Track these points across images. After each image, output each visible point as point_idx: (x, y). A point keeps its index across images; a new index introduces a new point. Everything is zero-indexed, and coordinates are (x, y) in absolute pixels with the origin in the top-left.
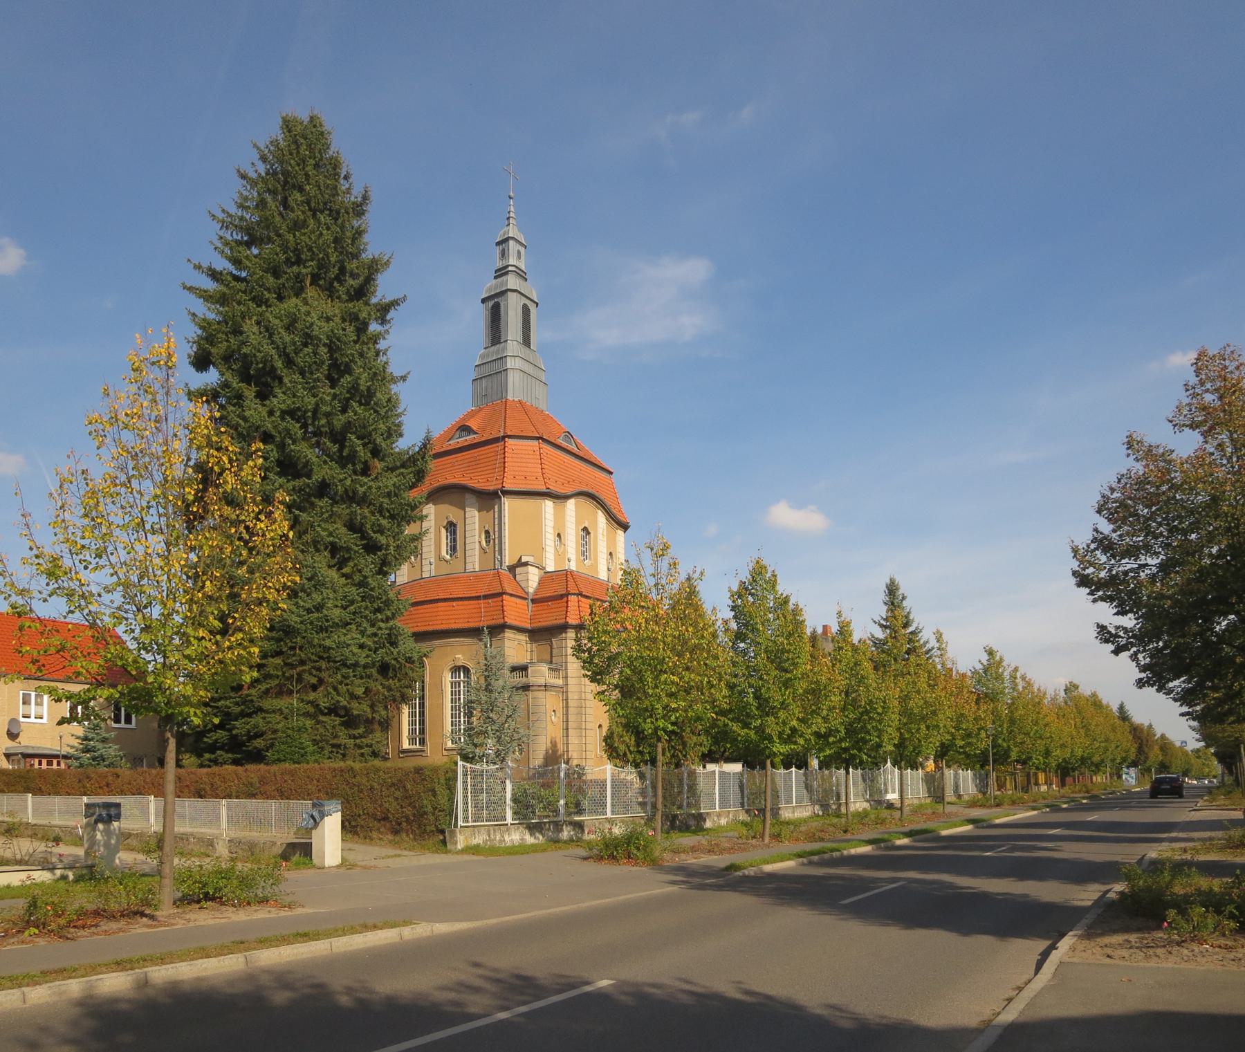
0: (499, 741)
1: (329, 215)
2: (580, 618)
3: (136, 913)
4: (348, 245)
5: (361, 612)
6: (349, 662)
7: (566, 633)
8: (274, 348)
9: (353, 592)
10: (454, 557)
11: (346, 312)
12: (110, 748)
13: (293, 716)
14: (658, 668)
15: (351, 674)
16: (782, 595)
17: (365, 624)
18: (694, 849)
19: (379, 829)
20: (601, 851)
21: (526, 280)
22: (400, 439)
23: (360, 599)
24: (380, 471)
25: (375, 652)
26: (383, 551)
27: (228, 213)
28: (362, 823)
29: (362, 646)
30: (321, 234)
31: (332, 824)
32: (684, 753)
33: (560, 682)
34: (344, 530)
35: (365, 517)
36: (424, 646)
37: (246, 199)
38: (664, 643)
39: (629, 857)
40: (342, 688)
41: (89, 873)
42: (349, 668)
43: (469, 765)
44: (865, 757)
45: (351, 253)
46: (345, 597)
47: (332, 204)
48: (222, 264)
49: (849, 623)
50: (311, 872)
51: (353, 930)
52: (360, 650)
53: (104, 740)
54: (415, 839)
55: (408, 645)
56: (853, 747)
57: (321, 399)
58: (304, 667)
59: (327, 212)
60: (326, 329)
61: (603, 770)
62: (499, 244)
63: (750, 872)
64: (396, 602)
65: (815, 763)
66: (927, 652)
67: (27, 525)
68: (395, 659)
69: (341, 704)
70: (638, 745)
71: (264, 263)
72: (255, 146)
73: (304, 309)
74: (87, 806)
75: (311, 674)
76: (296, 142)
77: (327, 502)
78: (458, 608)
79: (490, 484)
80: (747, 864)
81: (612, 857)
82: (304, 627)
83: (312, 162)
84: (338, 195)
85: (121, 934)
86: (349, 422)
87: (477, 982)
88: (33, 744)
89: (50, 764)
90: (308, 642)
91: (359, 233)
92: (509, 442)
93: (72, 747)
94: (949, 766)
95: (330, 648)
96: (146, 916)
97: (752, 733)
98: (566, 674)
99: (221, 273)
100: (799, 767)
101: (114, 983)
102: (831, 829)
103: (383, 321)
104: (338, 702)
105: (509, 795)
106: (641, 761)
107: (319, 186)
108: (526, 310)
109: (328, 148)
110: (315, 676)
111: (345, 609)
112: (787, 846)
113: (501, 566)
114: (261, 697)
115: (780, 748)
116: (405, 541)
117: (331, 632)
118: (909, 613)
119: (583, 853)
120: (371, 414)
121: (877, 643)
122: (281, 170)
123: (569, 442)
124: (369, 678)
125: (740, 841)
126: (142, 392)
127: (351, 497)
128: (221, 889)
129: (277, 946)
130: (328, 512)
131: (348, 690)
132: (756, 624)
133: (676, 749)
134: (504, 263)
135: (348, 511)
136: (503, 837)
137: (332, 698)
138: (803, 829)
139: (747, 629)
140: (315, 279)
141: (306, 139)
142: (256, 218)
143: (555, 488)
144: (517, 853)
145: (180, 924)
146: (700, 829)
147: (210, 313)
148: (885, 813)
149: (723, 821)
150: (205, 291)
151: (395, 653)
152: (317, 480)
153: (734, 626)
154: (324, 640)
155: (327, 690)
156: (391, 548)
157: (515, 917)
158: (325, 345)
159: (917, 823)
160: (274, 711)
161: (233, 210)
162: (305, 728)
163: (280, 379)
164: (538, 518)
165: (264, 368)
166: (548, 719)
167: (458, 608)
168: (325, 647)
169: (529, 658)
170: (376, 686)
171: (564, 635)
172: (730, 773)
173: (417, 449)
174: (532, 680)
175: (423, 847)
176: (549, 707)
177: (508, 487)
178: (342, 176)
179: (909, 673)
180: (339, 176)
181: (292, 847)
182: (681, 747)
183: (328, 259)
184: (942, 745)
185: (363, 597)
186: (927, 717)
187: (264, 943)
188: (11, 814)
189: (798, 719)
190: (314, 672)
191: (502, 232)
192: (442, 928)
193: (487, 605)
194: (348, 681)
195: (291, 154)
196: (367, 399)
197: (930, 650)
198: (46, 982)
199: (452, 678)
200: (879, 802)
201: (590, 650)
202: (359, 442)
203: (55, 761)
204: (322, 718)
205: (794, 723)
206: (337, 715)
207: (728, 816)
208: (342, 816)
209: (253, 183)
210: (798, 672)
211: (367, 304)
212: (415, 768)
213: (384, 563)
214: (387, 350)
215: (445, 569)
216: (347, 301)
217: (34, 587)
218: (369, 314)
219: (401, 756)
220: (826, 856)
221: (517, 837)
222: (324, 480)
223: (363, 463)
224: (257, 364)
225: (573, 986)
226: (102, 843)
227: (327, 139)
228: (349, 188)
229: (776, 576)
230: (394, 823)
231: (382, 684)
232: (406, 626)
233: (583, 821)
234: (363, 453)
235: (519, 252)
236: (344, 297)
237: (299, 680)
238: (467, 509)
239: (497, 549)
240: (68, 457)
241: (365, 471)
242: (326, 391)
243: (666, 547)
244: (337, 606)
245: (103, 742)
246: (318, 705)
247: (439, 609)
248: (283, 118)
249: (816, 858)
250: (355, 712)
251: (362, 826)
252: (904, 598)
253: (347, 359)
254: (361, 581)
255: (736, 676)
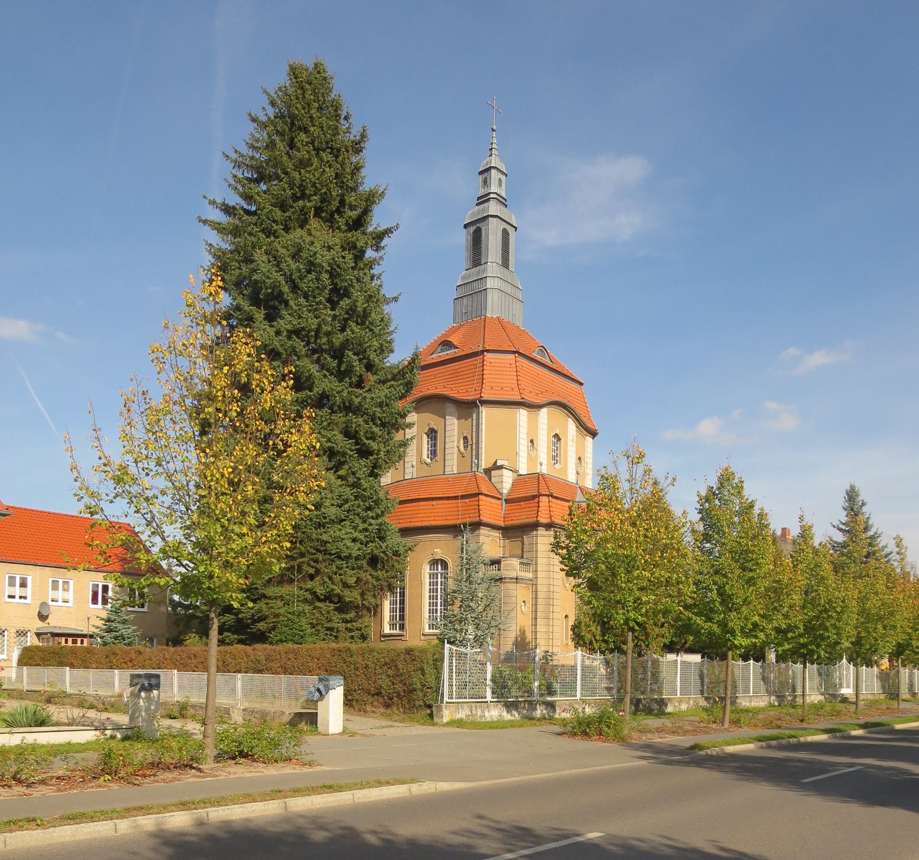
0: (477, 627)
1: (331, 153)
2: (550, 517)
3: (186, 766)
4: (347, 181)
5: (354, 510)
6: (343, 555)
7: (537, 530)
8: (281, 275)
9: (348, 492)
10: (434, 460)
11: (345, 241)
12: (129, 628)
13: (293, 602)
14: (630, 565)
15: (345, 566)
16: (747, 500)
17: (357, 520)
18: (659, 730)
19: (372, 703)
20: (573, 728)
21: (506, 206)
22: (391, 355)
23: (353, 498)
24: (373, 384)
25: (366, 545)
26: (375, 456)
27: (240, 153)
28: (357, 697)
29: (354, 540)
30: (324, 171)
31: (336, 696)
32: (647, 643)
33: (530, 575)
34: (340, 437)
35: (359, 425)
36: (409, 541)
37: (257, 141)
38: (637, 541)
39: (601, 734)
40: (337, 578)
41: (132, 735)
42: (343, 560)
43: (454, 648)
44: (822, 653)
45: (350, 187)
46: (340, 496)
47: (333, 143)
48: (234, 200)
49: (810, 527)
50: (319, 737)
51: (369, 785)
52: (353, 544)
53: (124, 622)
54: (405, 712)
55: (395, 540)
56: (811, 643)
57: (323, 320)
58: (303, 560)
59: (329, 150)
60: (328, 257)
61: (577, 657)
62: (481, 173)
63: (714, 751)
64: (385, 501)
65: (772, 657)
66: (886, 556)
67: (98, 439)
68: (384, 552)
69: (335, 592)
70: (603, 635)
71: (273, 198)
72: (265, 92)
73: (308, 239)
74: (132, 676)
75: (309, 565)
76: (302, 88)
77: (326, 412)
78: (438, 506)
79: (469, 394)
80: (710, 744)
81: (585, 733)
82: (304, 524)
83: (316, 105)
84: (339, 134)
85: (177, 782)
86: (347, 340)
87: (484, 831)
88: (59, 625)
89: (75, 642)
90: (308, 537)
91: (357, 168)
92: (488, 356)
93: (97, 627)
94: (904, 666)
95: (327, 542)
96: (194, 768)
97: (715, 628)
98: (536, 568)
99: (234, 208)
100: (757, 660)
101: (179, 820)
102: (789, 718)
103: (378, 248)
104: (333, 590)
105: (489, 676)
106: (606, 649)
107: (322, 127)
108: (505, 233)
109: (331, 91)
110: (312, 567)
111: (340, 507)
112: (746, 731)
113: (478, 469)
114: (264, 585)
115: (742, 641)
116: (394, 446)
117: (328, 528)
118: (868, 518)
119: (557, 729)
120: (366, 333)
121: (836, 546)
122: (288, 114)
123: (544, 356)
124: (360, 569)
125: (702, 725)
126: (194, 325)
127: (348, 408)
128: (253, 748)
129: (309, 795)
130: (326, 420)
131: (341, 580)
132: (722, 526)
133: (639, 640)
134: (487, 191)
135: (343, 419)
136: (483, 713)
137: (327, 587)
138: (761, 717)
139: (713, 531)
140: (318, 211)
141: (310, 84)
142: (264, 158)
143: (530, 398)
144: (496, 728)
145: (223, 776)
146: (661, 713)
147: (224, 243)
148: (840, 706)
149: (684, 707)
150: (219, 224)
151: (384, 547)
152: (318, 392)
153: (700, 527)
154: (321, 535)
155: (323, 580)
156: (382, 453)
157: (506, 780)
158: (327, 271)
159: (872, 717)
160: (276, 598)
161: (245, 150)
162: (305, 613)
163: (286, 303)
164: (513, 426)
165: (272, 293)
166: (519, 609)
167: (438, 506)
168: (322, 541)
169: (501, 553)
170: (365, 576)
171: (535, 532)
172: (691, 663)
173: (406, 363)
174: (504, 573)
175: (412, 720)
176: (520, 599)
177: (486, 397)
178: (343, 117)
179: (868, 576)
180: (340, 118)
181: (299, 717)
182: (643, 638)
183: (330, 194)
184: (899, 645)
185: (355, 496)
186: (885, 617)
187: (297, 792)
188: (51, 684)
189: (759, 615)
190: (312, 564)
191: (485, 162)
192: (445, 786)
193: (464, 504)
194: (342, 572)
195: (297, 98)
196: (363, 318)
197: (889, 554)
198: (131, 816)
199: (430, 570)
200: (833, 696)
201: (567, 547)
202: (355, 358)
203: (79, 640)
204: (318, 604)
205: (756, 618)
206: (331, 602)
207: (688, 703)
208: (344, 690)
209: (264, 126)
210: (761, 572)
211: (364, 233)
212: (406, 650)
213: (375, 466)
214: (381, 274)
215: (426, 472)
216: (346, 231)
217: (103, 490)
218: (366, 243)
219: (382, 639)
220: (784, 742)
221: (495, 713)
222: (324, 391)
223: (358, 377)
224: (266, 289)
225: (566, 837)
226: (144, 708)
227: (329, 83)
228: (349, 128)
229: (742, 482)
230: (386, 698)
231: (371, 575)
232: (393, 523)
233: (555, 701)
234: (359, 368)
235: (500, 180)
236: (344, 227)
237: (300, 570)
238: (447, 417)
239: (474, 453)
240: (132, 380)
241: (360, 384)
242: (327, 313)
243: (642, 456)
244: (333, 505)
245: (123, 623)
246: (316, 592)
247: (421, 508)
248: (290, 66)
249: (774, 743)
250: (347, 599)
251: (357, 700)
252: (863, 504)
253: (346, 284)
254: (355, 482)
255: (701, 573)
